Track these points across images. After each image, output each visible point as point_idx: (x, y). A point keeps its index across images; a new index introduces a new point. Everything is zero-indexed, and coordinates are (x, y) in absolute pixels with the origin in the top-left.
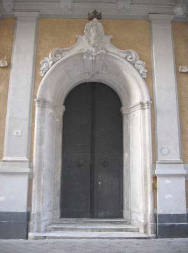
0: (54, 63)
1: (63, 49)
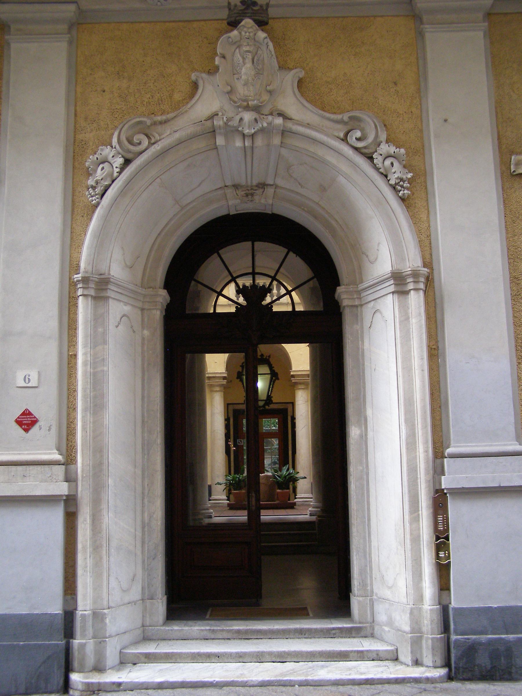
0: (127, 162)
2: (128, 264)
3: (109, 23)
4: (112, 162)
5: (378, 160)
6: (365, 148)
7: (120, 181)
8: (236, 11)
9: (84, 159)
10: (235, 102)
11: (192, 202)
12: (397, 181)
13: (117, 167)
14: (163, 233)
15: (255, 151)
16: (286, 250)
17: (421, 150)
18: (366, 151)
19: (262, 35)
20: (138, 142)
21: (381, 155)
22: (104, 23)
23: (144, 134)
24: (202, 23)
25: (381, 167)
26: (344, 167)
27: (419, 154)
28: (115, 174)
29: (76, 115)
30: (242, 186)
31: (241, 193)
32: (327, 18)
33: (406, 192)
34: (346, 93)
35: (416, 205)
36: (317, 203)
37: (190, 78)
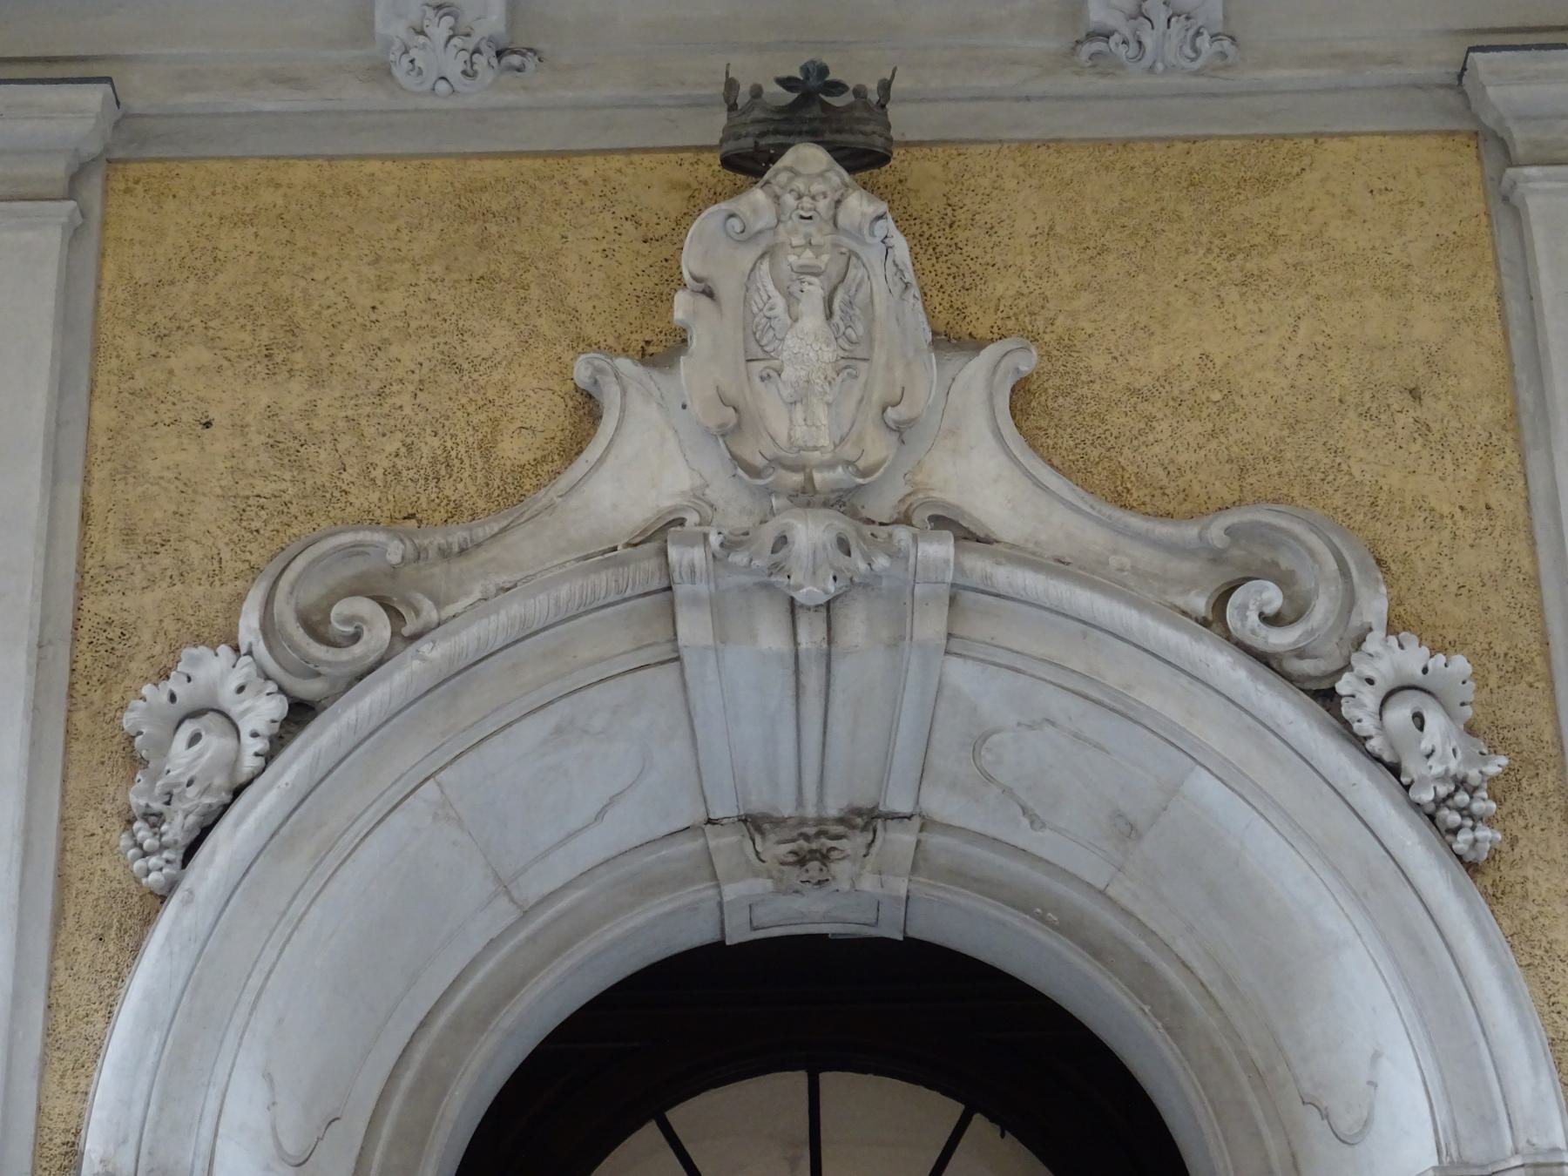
0: (301, 712)
1: (814, 846)
2: (290, 1147)
3: (233, 159)
4: (234, 711)
6: (1300, 654)
7: (269, 788)
8: (757, 114)
9: (116, 697)
10: (754, 472)
11: (568, 886)
12: (1443, 790)
13: (255, 735)
14: (442, 1020)
15: (842, 670)
16: (956, 1109)
17: (1538, 660)
18: (1306, 666)
19: (859, 206)
20: (350, 630)
21: (1370, 681)
22: (219, 159)
23: (373, 598)
24: (617, 161)
25: (1373, 731)
27: (1531, 679)
28: (249, 763)
29: (85, 518)
30: (778, 822)
31: (775, 849)
32: (1126, 143)
33: (1484, 833)
34: (1213, 434)
35: (1530, 886)
36: (1102, 893)
37: (565, 373)
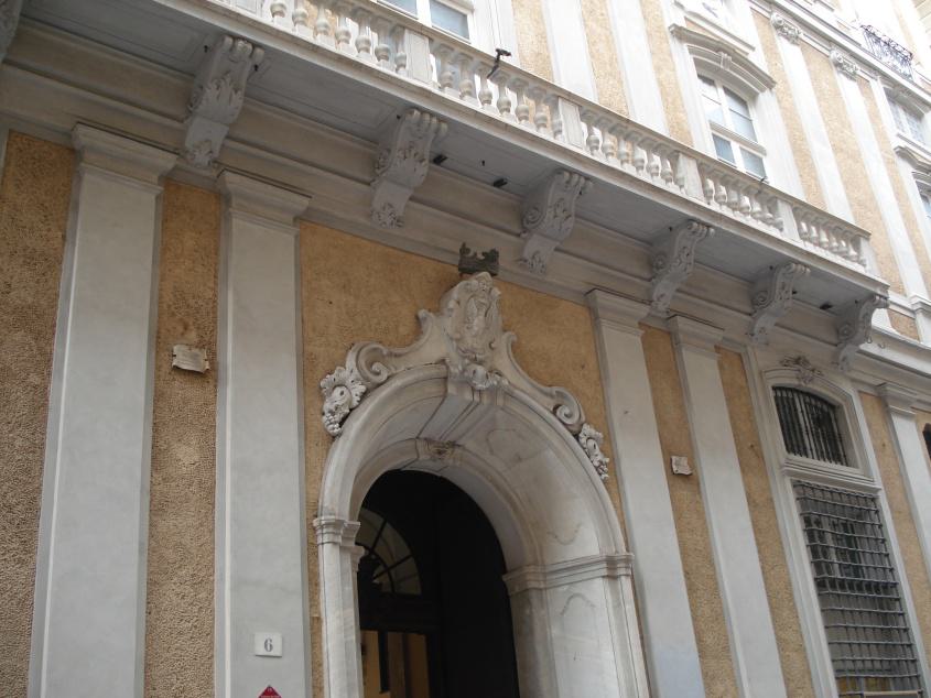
5: (583, 440)
26: (556, 441)
28: (355, 403)
31: (433, 449)
